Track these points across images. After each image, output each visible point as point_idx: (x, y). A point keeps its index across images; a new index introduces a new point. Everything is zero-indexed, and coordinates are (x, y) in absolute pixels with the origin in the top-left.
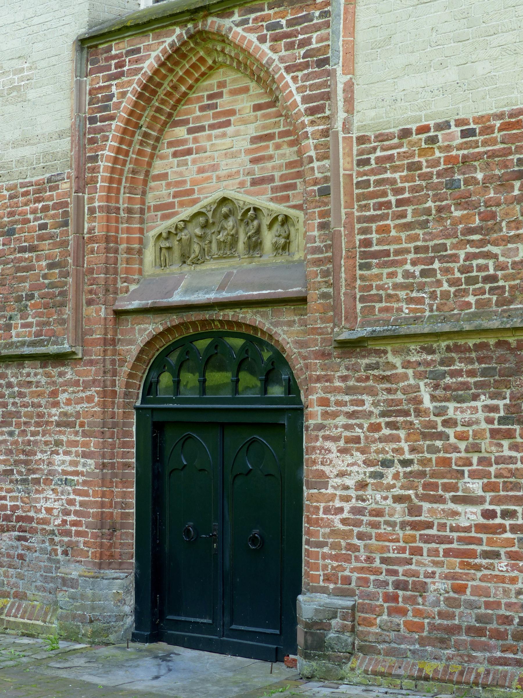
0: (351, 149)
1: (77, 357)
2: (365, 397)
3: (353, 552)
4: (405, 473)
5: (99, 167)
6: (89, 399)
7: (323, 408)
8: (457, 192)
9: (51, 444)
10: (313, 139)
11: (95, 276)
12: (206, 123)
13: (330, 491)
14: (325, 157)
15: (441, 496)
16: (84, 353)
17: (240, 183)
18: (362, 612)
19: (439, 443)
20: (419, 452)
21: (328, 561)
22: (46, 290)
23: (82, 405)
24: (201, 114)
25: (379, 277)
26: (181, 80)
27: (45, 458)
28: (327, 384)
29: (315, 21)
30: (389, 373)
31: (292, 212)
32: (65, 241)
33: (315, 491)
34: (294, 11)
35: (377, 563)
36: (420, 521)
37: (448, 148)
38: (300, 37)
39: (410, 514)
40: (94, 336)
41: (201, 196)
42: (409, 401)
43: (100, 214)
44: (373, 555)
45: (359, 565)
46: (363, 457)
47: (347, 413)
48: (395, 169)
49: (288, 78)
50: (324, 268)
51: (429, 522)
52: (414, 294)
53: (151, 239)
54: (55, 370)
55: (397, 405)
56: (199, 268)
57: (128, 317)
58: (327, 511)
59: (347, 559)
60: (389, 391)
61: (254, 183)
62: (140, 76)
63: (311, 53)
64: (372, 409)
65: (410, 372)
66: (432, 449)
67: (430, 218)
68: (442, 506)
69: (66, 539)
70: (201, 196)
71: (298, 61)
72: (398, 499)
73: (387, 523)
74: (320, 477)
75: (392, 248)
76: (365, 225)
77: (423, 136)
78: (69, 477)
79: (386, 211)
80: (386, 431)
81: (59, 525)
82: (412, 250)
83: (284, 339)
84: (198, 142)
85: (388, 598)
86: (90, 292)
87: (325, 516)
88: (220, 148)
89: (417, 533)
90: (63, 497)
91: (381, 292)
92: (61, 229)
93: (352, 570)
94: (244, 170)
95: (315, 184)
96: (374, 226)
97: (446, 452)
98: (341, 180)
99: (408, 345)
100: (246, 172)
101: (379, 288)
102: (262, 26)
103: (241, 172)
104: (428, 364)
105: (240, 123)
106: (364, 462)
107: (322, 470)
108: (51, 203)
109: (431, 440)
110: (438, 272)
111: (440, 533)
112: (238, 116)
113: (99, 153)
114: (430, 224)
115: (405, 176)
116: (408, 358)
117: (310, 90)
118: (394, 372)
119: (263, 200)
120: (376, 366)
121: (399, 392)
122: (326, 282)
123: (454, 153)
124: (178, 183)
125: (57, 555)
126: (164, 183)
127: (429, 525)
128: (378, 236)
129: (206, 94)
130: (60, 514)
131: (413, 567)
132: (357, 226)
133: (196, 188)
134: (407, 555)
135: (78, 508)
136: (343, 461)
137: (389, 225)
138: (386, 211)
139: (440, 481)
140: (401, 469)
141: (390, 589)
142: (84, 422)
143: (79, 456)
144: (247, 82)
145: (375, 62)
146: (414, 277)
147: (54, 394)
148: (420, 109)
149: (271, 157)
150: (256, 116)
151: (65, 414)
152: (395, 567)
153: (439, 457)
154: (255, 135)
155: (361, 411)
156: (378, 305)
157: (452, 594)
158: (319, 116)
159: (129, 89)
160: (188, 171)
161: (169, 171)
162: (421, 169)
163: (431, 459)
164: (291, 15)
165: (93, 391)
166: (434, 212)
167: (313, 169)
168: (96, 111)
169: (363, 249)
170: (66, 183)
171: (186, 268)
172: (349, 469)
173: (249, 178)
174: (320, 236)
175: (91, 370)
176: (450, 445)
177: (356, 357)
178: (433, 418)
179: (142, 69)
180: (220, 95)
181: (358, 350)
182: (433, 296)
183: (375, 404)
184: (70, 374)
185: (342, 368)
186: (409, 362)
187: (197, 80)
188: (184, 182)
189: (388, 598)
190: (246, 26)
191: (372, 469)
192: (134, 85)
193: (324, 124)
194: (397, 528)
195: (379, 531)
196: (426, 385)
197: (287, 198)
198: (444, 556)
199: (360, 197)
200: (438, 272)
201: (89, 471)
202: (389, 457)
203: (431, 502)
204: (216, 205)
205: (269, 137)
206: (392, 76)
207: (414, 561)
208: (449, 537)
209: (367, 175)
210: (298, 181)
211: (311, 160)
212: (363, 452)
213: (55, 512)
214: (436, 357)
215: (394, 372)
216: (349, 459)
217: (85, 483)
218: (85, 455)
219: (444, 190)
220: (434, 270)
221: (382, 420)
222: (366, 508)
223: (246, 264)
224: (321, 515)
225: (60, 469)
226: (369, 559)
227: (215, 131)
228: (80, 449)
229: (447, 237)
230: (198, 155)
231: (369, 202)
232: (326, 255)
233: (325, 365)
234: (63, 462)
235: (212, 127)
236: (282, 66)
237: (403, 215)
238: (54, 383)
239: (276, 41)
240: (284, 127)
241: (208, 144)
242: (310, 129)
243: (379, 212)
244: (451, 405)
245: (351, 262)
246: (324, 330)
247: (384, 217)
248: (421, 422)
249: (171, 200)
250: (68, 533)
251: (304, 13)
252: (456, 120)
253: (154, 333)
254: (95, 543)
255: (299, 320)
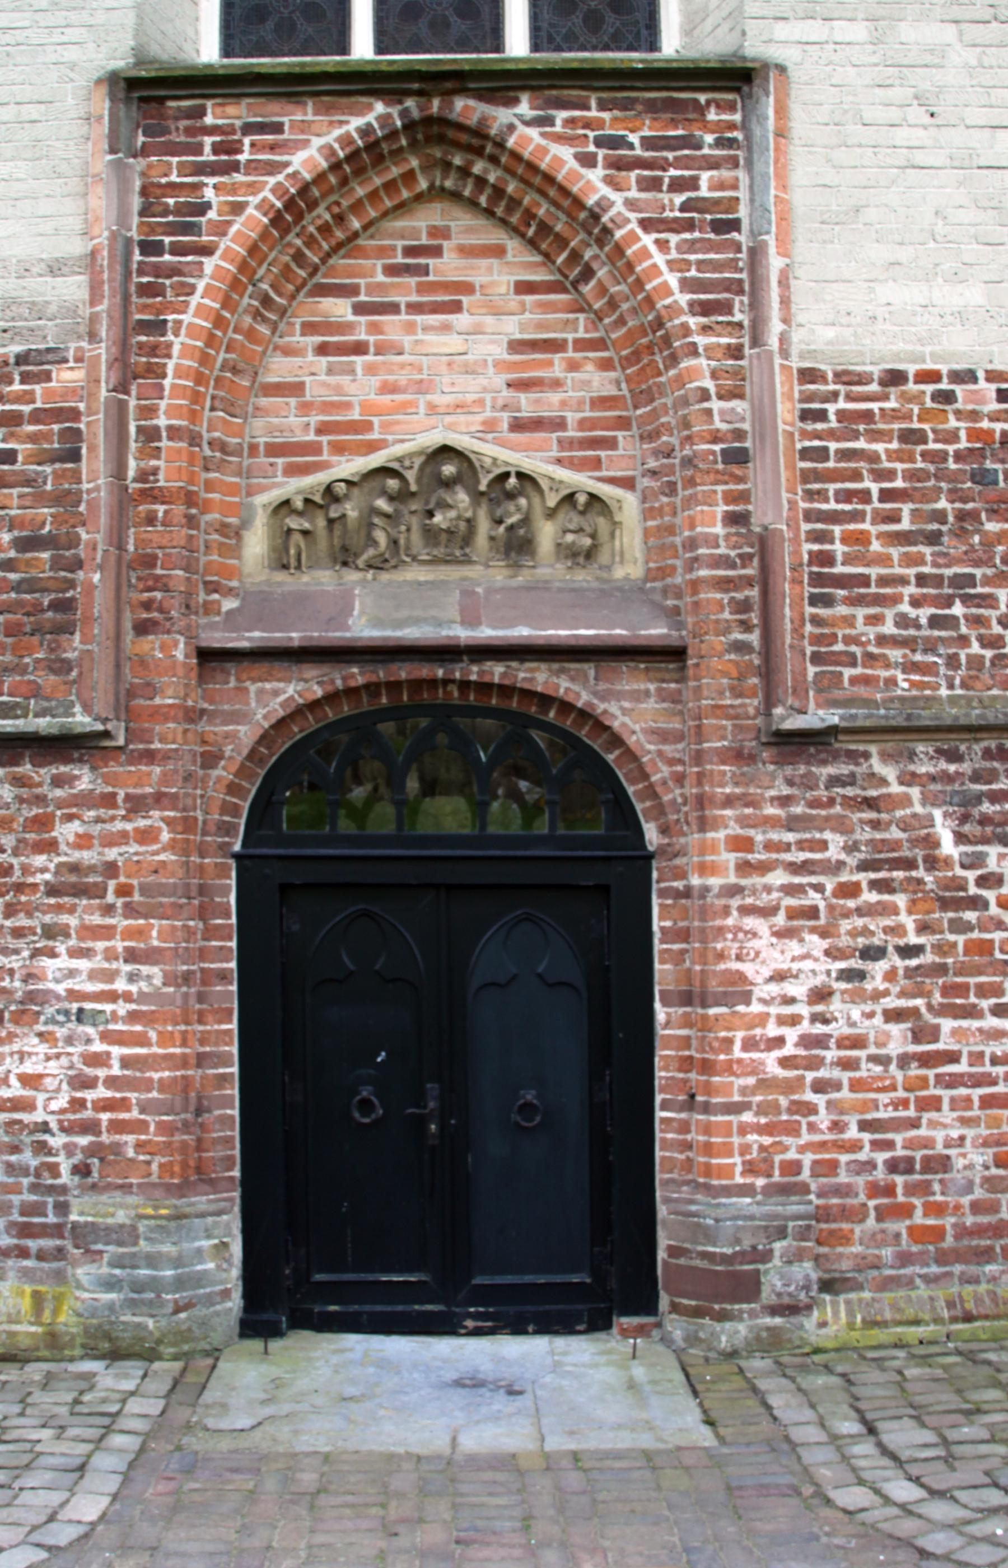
0: (791, 388)
1: (113, 744)
2: (827, 835)
3: (804, 1116)
4: (907, 969)
5: (169, 345)
6: (146, 836)
7: (740, 855)
8: (991, 492)
9: (35, 934)
10: (709, 358)
11: (159, 571)
12: (402, 300)
13: (756, 1008)
14: (736, 394)
15: (974, 1006)
16: (131, 735)
17: (484, 423)
18: (827, 1221)
19: (970, 916)
20: (934, 932)
21: (752, 1137)
22: (13, 595)
23: (124, 849)
24: (388, 280)
25: (849, 621)
26: (357, 207)
27: (15, 965)
28: (748, 811)
29: (706, 151)
30: (873, 793)
31: (605, 490)
32: (69, 492)
33: (723, 1010)
34: (657, 124)
35: (853, 1132)
36: (937, 1052)
37: (974, 415)
38: (673, 172)
39: (917, 1039)
40: (158, 701)
41: (390, 438)
42: (914, 842)
43: (170, 444)
44: (845, 1118)
45: (817, 1138)
46: (825, 944)
47: (791, 864)
48: (876, 436)
49: (648, 240)
50: (739, 596)
51: (953, 1052)
52: (918, 657)
53: (260, 511)
54: (42, 771)
55: (893, 850)
56: (385, 577)
57: (228, 665)
58: (749, 1045)
59: (793, 1130)
60: (876, 825)
61: (518, 426)
62: (280, 178)
63: (699, 205)
64: (843, 856)
65: (915, 792)
66: (959, 927)
67: (944, 528)
68: (975, 1024)
69: (84, 1141)
70: (390, 438)
71: (668, 214)
72: (894, 1016)
73: (873, 1059)
74: (733, 984)
75: (874, 572)
76: (819, 526)
77: (929, 388)
78: (88, 1006)
79: (860, 507)
80: (870, 897)
81: (62, 1111)
82: (913, 580)
83: (624, 725)
84: (382, 333)
85: (875, 1190)
86: (147, 606)
87: (745, 1056)
88: (435, 350)
89: (931, 1073)
90: (70, 1050)
91: (853, 648)
92: (57, 466)
93: (802, 1149)
94: (494, 399)
95: (715, 440)
96: (837, 530)
97: (982, 929)
98: (781, 439)
99: (910, 745)
100: (500, 403)
101: (848, 640)
102: (586, 136)
103: (488, 403)
104: (947, 778)
105: (484, 311)
106: (827, 953)
107: (737, 971)
108: (26, 409)
109: (956, 911)
110: (962, 621)
111: (974, 1070)
112: (478, 296)
113: (170, 317)
114: (945, 539)
115: (896, 451)
116: (912, 767)
117: (699, 270)
118: (884, 790)
119: (537, 460)
120: (851, 780)
121: (893, 828)
122: (742, 622)
123: (985, 424)
124: (328, 407)
125: (57, 1175)
126: (293, 401)
127: (953, 1057)
128: (846, 549)
129: (400, 244)
130: (65, 1086)
131: (923, 1132)
132: (805, 527)
133: (376, 420)
134: (911, 1113)
135: (116, 1070)
136: (782, 952)
137: (868, 532)
138: (860, 507)
139: (972, 980)
140: (900, 963)
141: (880, 1174)
142: (131, 886)
143: (117, 959)
144: (497, 236)
145: (829, 246)
146: (918, 627)
147: (43, 823)
148: (921, 341)
149: (557, 384)
150: (523, 304)
151: (74, 868)
152: (889, 1136)
153: (972, 940)
154: (518, 336)
155: (821, 861)
156: (848, 672)
157: (994, 1171)
158: (721, 319)
159: (250, 199)
160: (359, 386)
161: (308, 379)
162: (926, 442)
163: (954, 945)
164: (650, 129)
165: (155, 818)
166: (951, 519)
167: (709, 412)
168: (159, 230)
169: (815, 569)
170: (71, 369)
171: (352, 576)
172: (795, 966)
173: (505, 416)
174: (727, 537)
175: (149, 774)
176: (991, 918)
177: (808, 763)
178: (959, 872)
179: (287, 164)
180: (436, 251)
181: (812, 750)
182: (953, 662)
183: (851, 848)
184: (85, 779)
185: (779, 782)
186: (914, 774)
187: (385, 214)
188: (347, 406)
189: (875, 1190)
190: (548, 129)
191: (842, 965)
192: (269, 191)
193: (730, 335)
194: (893, 1067)
195: (857, 1074)
196: (946, 815)
197: (596, 464)
198: (981, 1108)
199: (807, 476)
200: (962, 621)
201: (146, 989)
202: (876, 941)
203: (955, 1017)
204: (422, 458)
205: (555, 346)
206: (865, 276)
207: (924, 1121)
208: (990, 1074)
209: (821, 439)
210: (620, 434)
211: (704, 395)
212: (824, 934)
213: (49, 1083)
214: (966, 767)
215: (884, 790)
216: (794, 947)
217: (133, 1017)
218: (131, 956)
219: (969, 484)
220: (955, 618)
221: (863, 878)
222: (830, 1036)
223: (499, 575)
224: (737, 1053)
225: (60, 989)
226: (837, 1126)
227: (424, 317)
228: (119, 945)
229: (977, 563)
230: (379, 358)
231: (826, 486)
232: (743, 572)
233: (743, 774)
234: (72, 973)
235: (415, 308)
236: (633, 216)
237: (894, 517)
238: (41, 800)
239: (619, 169)
240: (587, 331)
241: (407, 340)
242: (701, 341)
243: (847, 507)
244: (993, 851)
245: (797, 589)
246: (740, 711)
247: (857, 516)
248: (937, 881)
249: (311, 437)
250: (90, 1127)
251: (680, 132)
252: (987, 372)
253: (301, 701)
254: (169, 1144)
255: (659, 690)
